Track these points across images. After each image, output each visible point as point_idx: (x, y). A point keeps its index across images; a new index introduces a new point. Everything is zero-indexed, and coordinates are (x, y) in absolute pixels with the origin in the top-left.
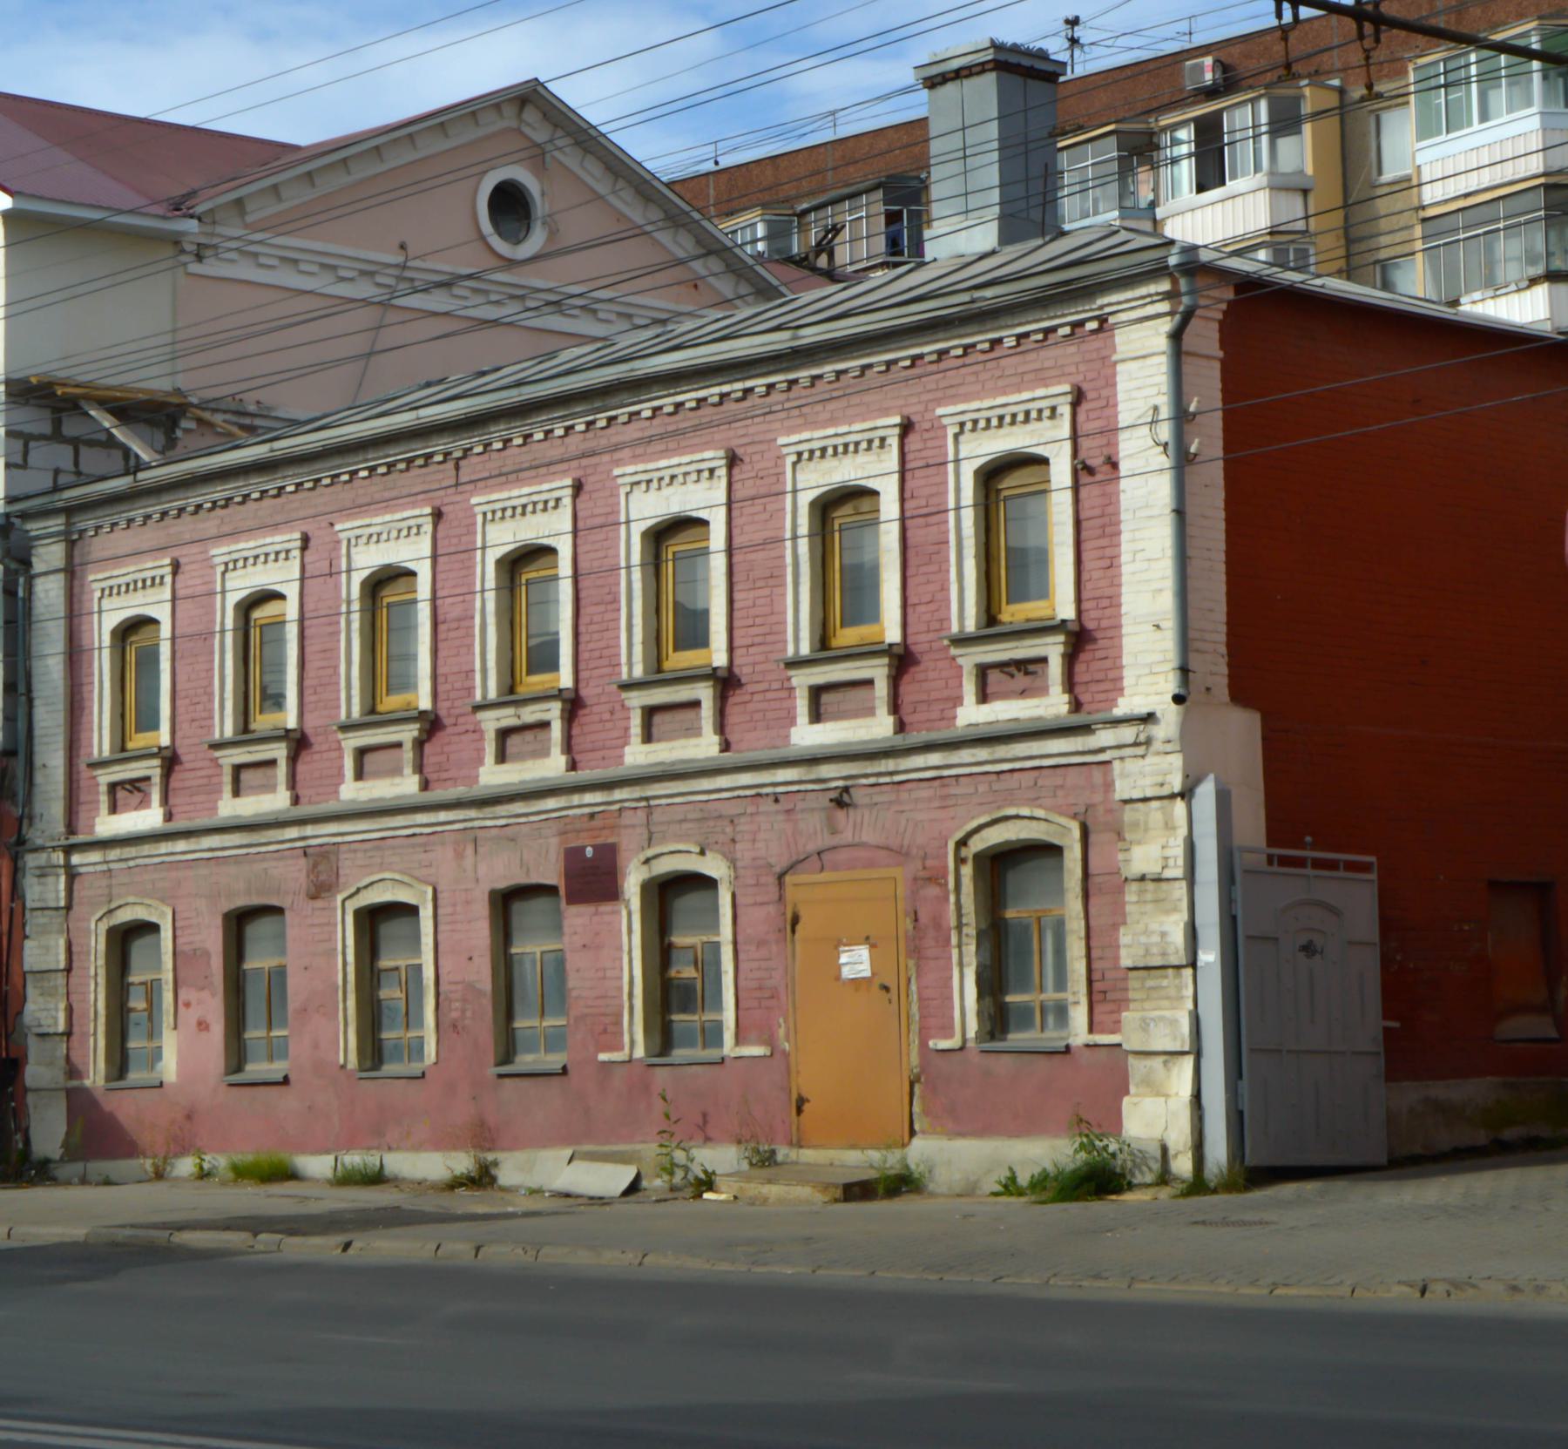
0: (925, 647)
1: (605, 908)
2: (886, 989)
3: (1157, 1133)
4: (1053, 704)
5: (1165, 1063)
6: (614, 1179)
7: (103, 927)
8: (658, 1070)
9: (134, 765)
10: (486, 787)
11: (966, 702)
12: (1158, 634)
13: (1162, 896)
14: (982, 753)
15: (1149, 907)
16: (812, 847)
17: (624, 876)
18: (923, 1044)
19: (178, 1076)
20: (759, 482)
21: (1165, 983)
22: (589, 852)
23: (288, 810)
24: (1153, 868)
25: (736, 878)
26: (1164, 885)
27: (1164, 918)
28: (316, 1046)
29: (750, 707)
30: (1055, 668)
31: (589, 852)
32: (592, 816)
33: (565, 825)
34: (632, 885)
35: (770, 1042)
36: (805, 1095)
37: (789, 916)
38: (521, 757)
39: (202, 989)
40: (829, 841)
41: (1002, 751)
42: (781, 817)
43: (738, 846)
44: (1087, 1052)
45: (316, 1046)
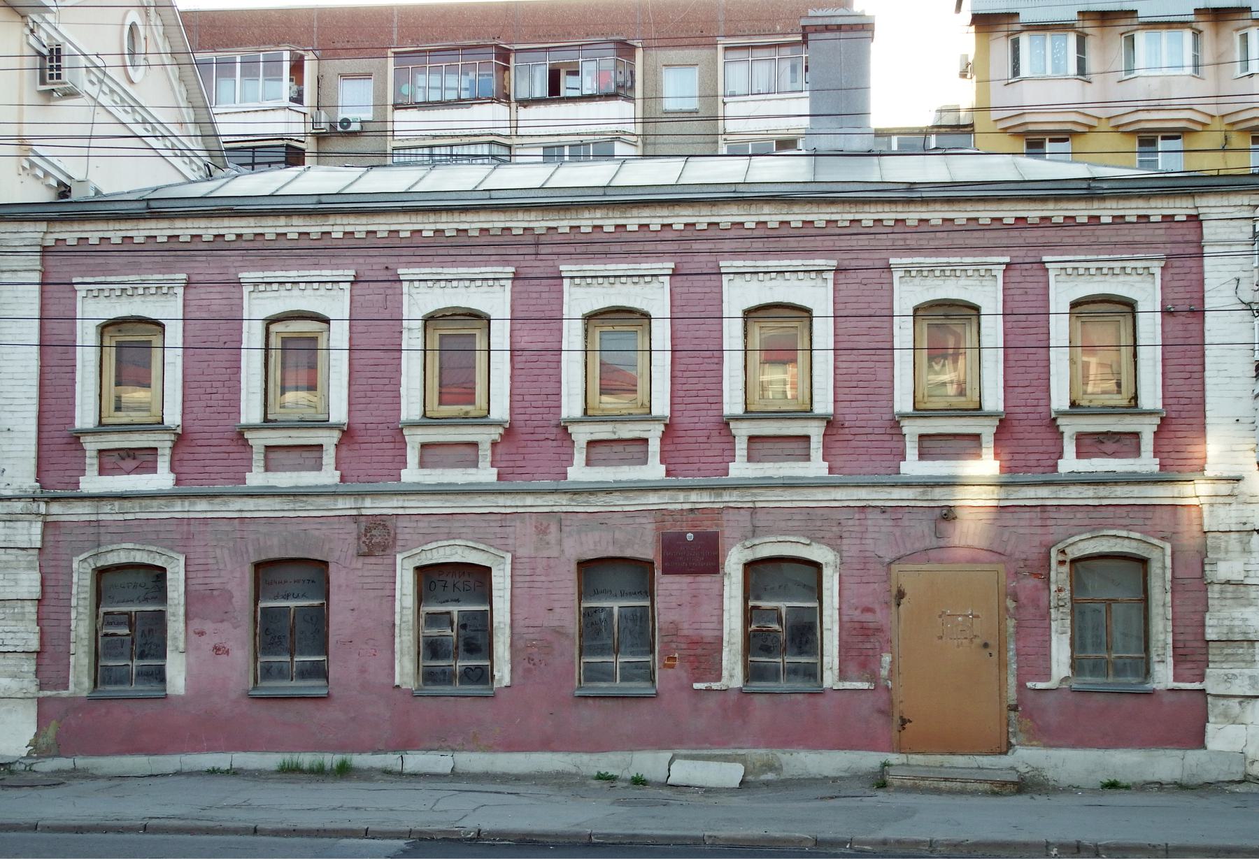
0: (522, 423)
1: (705, 580)
2: (986, 645)
3: (1238, 748)
4: (1147, 463)
5: (1240, 703)
6: (732, 774)
7: (92, 564)
8: (757, 698)
9: (136, 436)
10: (574, 482)
11: (1066, 455)
12: (1239, 426)
13: (1240, 595)
14: (1089, 491)
15: (1228, 602)
16: (918, 546)
17: (725, 557)
18: (1021, 686)
19: (187, 687)
20: (862, 287)
21: (1241, 651)
22: (690, 537)
23: (336, 485)
24: (1237, 576)
25: (842, 563)
26: (1242, 588)
27: (1243, 610)
28: (363, 671)
29: (854, 444)
30: (654, 446)
31: (690, 537)
32: (692, 510)
33: (661, 515)
34: (734, 560)
35: (874, 677)
36: (906, 717)
37: (894, 591)
38: (435, 465)
39: (222, 621)
40: (935, 543)
41: (1102, 491)
42: (889, 523)
43: (845, 541)
44: (1170, 694)
45: (363, 671)
